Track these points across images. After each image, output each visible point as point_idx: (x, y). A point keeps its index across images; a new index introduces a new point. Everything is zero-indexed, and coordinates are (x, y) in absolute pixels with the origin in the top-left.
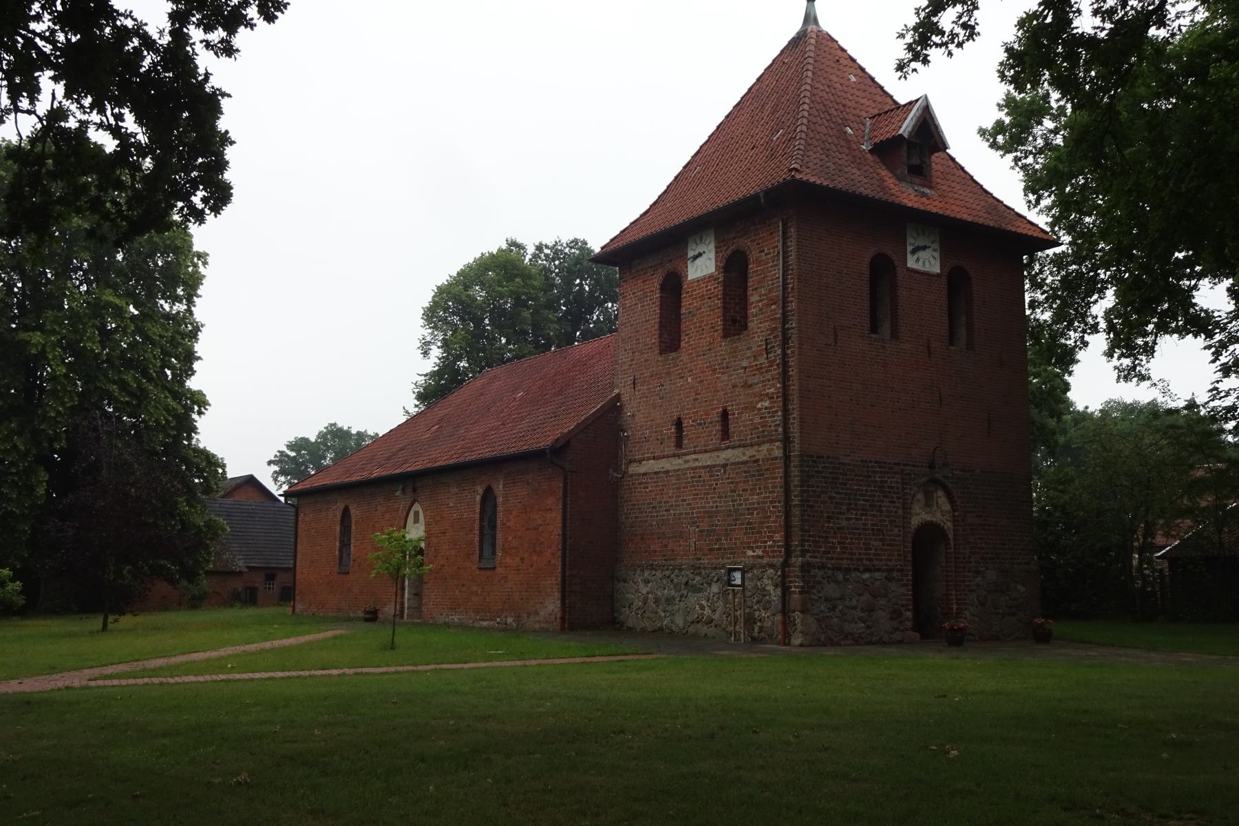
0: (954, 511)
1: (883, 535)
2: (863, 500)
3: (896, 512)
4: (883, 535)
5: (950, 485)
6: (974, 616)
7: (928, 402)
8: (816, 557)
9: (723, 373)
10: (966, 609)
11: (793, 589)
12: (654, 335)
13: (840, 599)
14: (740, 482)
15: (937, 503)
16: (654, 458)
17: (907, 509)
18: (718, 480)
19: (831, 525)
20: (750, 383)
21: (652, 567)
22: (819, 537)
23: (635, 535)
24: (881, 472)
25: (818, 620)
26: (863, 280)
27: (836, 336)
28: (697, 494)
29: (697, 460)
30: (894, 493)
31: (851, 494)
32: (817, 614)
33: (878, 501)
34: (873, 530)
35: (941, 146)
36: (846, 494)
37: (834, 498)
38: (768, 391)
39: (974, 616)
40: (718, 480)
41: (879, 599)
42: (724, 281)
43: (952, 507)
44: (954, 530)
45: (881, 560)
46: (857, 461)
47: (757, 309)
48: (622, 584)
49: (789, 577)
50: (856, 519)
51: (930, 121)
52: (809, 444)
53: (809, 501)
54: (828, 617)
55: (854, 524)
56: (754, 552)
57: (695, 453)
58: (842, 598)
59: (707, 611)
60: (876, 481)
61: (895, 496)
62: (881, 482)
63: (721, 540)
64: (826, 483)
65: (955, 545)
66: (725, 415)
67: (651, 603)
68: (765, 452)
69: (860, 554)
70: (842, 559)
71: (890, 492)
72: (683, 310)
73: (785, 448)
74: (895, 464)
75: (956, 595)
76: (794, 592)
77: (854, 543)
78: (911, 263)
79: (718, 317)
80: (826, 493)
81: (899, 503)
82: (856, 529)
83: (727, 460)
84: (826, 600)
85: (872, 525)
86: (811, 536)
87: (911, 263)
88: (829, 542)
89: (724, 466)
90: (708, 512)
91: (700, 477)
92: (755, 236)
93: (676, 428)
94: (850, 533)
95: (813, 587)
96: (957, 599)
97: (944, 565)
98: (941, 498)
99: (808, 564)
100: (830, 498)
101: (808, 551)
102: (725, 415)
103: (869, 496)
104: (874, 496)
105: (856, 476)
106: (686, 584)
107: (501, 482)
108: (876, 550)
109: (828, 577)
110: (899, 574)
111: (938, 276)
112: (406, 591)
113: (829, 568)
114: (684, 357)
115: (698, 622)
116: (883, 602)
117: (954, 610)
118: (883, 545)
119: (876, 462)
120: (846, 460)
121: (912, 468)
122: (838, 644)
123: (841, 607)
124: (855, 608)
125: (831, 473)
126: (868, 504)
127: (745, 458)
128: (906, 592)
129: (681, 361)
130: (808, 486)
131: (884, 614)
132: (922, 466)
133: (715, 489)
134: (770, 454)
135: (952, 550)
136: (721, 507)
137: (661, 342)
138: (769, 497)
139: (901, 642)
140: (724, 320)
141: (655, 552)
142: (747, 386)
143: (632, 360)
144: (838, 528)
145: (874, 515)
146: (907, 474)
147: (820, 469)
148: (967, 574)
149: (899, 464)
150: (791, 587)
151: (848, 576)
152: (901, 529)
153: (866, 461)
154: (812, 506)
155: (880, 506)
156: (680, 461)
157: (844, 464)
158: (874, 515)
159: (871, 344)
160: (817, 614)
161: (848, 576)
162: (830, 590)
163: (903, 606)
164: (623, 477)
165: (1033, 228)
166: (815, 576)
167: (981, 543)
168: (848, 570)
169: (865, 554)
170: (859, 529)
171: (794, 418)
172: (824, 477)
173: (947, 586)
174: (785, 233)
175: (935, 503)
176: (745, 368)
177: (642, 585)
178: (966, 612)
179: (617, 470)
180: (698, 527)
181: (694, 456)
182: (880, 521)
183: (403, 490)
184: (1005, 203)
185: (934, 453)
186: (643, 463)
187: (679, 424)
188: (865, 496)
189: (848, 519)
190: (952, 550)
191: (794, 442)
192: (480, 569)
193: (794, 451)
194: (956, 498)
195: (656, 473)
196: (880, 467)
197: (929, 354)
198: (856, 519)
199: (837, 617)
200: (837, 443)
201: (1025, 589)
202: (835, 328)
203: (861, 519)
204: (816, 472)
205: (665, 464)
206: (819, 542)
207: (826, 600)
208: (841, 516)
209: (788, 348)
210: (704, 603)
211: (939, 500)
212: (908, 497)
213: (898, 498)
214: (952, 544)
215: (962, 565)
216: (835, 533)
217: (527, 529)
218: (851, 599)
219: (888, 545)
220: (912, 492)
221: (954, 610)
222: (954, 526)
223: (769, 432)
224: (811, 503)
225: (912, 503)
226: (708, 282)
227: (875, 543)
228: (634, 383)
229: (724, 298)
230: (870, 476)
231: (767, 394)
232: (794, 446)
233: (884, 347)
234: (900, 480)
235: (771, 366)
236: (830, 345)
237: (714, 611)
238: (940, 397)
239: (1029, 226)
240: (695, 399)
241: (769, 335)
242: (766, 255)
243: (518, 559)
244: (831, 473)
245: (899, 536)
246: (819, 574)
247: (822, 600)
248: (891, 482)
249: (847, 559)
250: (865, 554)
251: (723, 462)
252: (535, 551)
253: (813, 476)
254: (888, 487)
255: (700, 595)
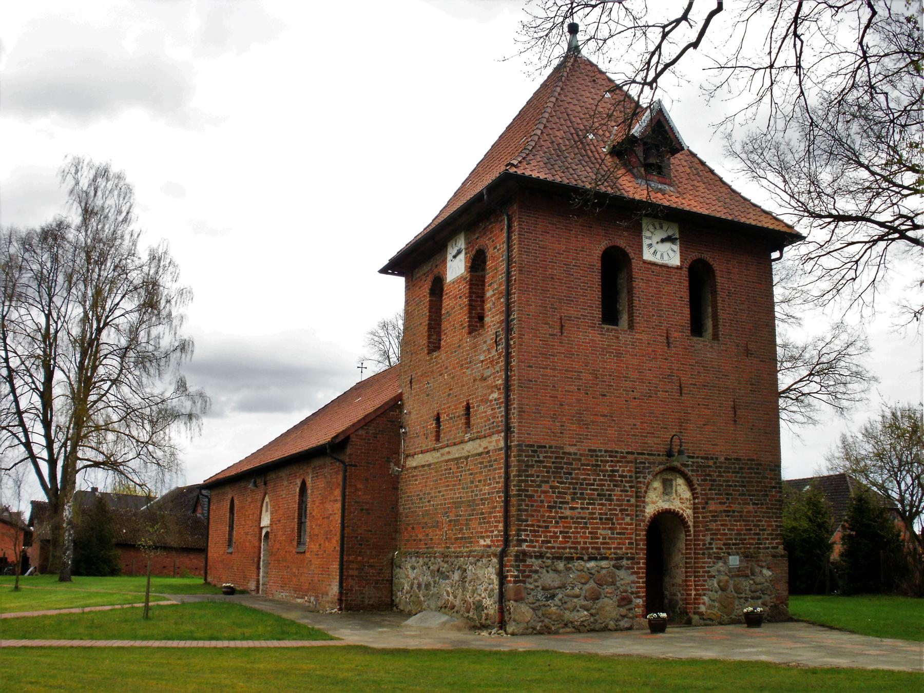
0: (694, 498)
1: (613, 524)
2: (591, 489)
3: (628, 501)
4: (613, 524)
5: (690, 473)
6: (713, 601)
7: (666, 392)
8: (534, 547)
9: (468, 368)
10: (704, 595)
11: (509, 579)
12: (424, 337)
13: (560, 588)
14: (476, 473)
15: (676, 491)
16: (422, 452)
17: (640, 498)
18: (462, 471)
19: (553, 514)
20: (485, 376)
21: (418, 555)
22: (539, 526)
23: (408, 525)
24: (612, 461)
25: (534, 609)
26: (595, 272)
27: (562, 326)
28: (448, 486)
29: (449, 453)
30: (626, 482)
31: (577, 483)
32: (533, 603)
33: (607, 490)
34: (601, 519)
35: (678, 146)
36: (571, 483)
37: (558, 487)
38: (497, 382)
39: (713, 601)
40: (462, 471)
41: (605, 587)
42: (471, 280)
43: (693, 494)
44: (694, 517)
45: (610, 549)
46: (585, 450)
47: (491, 303)
48: (398, 570)
49: (506, 566)
50: (582, 508)
51: (664, 123)
52: (528, 434)
53: (527, 491)
54: (544, 605)
55: (580, 513)
56: (485, 541)
57: (447, 446)
58: (563, 587)
59: (451, 598)
60: (607, 471)
61: (627, 485)
62: (611, 471)
63: (463, 529)
64: (548, 472)
65: (695, 531)
66: (468, 408)
67: (415, 586)
68: (494, 443)
69: (585, 543)
70: (565, 548)
71: (622, 481)
72: (443, 312)
73: (507, 439)
74: (628, 453)
75: (695, 581)
76: (510, 581)
77: (578, 533)
78: (647, 255)
79: (465, 315)
80: (547, 482)
81: (632, 491)
82: (582, 518)
83: (469, 452)
84: (544, 589)
85: (600, 514)
86: (528, 526)
87: (647, 255)
88: (550, 532)
89: (467, 458)
90: (455, 503)
91: (450, 469)
92: (491, 234)
93: (436, 424)
94: (574, 523)
95: (529, 576)
96: (695, 585)
97: (684, 551)
98: (680, 486)
99: (524, 553)
100: (552, 487)
101: (525, 541)
102: (468, 408)
103: (598, 485)
104: (604, 485)
105: (583, 465)
106: (438, 571)
107: (310, 476)
108: (604, 538)
109: (547, 567)
110: (629, 562)
111: (678, 268)
112: (261, 570)
113: (548, 558)
114: (443, 356)
115: (446, 607)
116: (609, 589)
117: (693, 596)
118: (613, 534)
119: (606, 451)
120: (572, 450)
121: (647, 457)
122: (556, 633)
123: (560, 596)
124: (577, 596)
125: (553, 463)
126: (596, 493)
127: (481, 450)
128: (637, 580)
129: (441, 359)
130: (527, 476)
131: (611, 602)
132: (659, 455)
133: (460, 480)
134: (497, 445)
135: (692, 537)
136: (464, 497)
137: (429, 342)
138: (495, 488)
139: (630, 628)
140: (470, 317)
141: (420, 540)
142: (483, 379)
143: (411, 361)
144: (561, 518)
145: (602, 504)
146: (641, 463)
147: (541, 459)
148: (706, 560)
149: (632, 453)
150: (507, 576)
151: (570, 565)
152: (634, 517)
153: (595, 451)
154: (532, 496)
155: (610, 495)
156: (438, 454)
157: (570, 454)
158: (602, 504)
159: (602, 334)
160: (533, 603)
161: (570, 565)
162: (549, 579)
163: (632, 593)
164: (402, 471)
165: (777, 223)
166: (532, 566)
167: (724, 530)
168: (570, 559)
169: (590, 543)
170: (584, 518)
171: (514, 408)
172: (545, 467)
173: (686, 572)
174: (510, 227)
175: (674, 491)
176: (482, 361)
177: (410, 571)
178: (704, 597)
179: (397, 464)
180: (448, 517)
181: (447, 449)
182: (610, 510)
183: (255, 483)
184: (752, 201)
185: (671, 441)
186: (416, 456)
187: (438, 419)
188: (593, 485)
189: (572, 509)
190: (692, 537)
191: (514, 432)
192: (298, 553)
193: (514, 441)
194: (696, 486)
195: (423, 466)
196: (610, 456)
197: (668, 343)
198: (582, 508)
199: (555, 605)
200: (561, 433)
201: (770, 573)
202: (561, 319)
203: (588, 509)
204: (536, 461)
205: (429, 458)
206: (538, 531)
207: (544, 589)
208: (565, 506)
209: (511, 339)
210: (449, 589)
211: (678, 488)
212: (642, 485)
213: (631, 487)
214: (692, 532)
215: (701, 552)
216: (557, 522)
217: (323, 518)
218: (573, 588)
219: (617, 534)
220: (646, 481)
221: (693, 596)
222: (694, 513)
223: (497, 423)
224: (529, 493)
225: (646, 492)
226: (460, 282)
227: (603, 532)
228: (411, 382)
229: (470, 296)
230: (600, 466)
231: (496, 386)
232: (514, 436)
233: (618, 338)
234: (633, 469)
235: (500, 358)
236: (556, 335)
237: (455, 597)
238: (680, 386)
239: (773, 221)
240: (449, 395)
241: (499, 327)
242: (498, 250)
243: (317, 544)
244: (553, 463)
245: (631, 524)
246: (536, 563)
247: (539, 589)
248: (623, 471)
249: (570, 548)
250: (590, 543)
251: (467, 454)
252: (327, 538)
253: (532, 466)
254: (620, 476)
255: (447, 581)
